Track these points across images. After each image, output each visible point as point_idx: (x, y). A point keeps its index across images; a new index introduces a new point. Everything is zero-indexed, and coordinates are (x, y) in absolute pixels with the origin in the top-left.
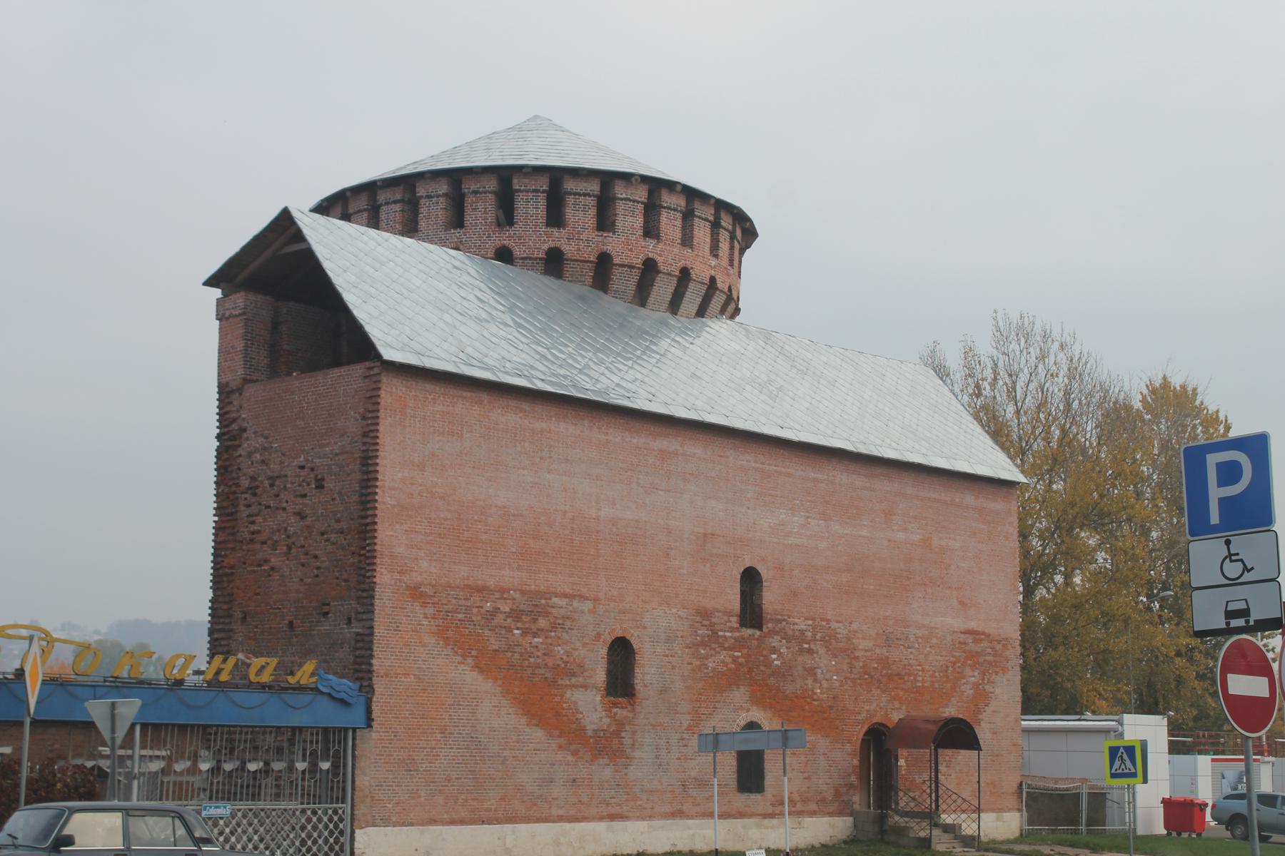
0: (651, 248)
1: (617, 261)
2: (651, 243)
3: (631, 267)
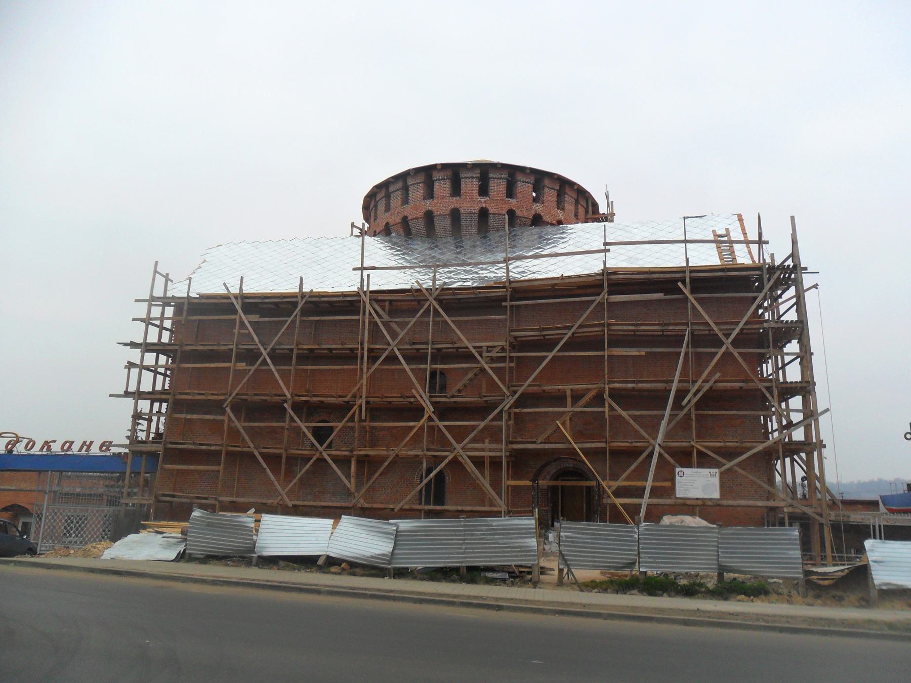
0: (429, 205)
1: (435, 214)
2: (428, 202)
3: (417, 218)
